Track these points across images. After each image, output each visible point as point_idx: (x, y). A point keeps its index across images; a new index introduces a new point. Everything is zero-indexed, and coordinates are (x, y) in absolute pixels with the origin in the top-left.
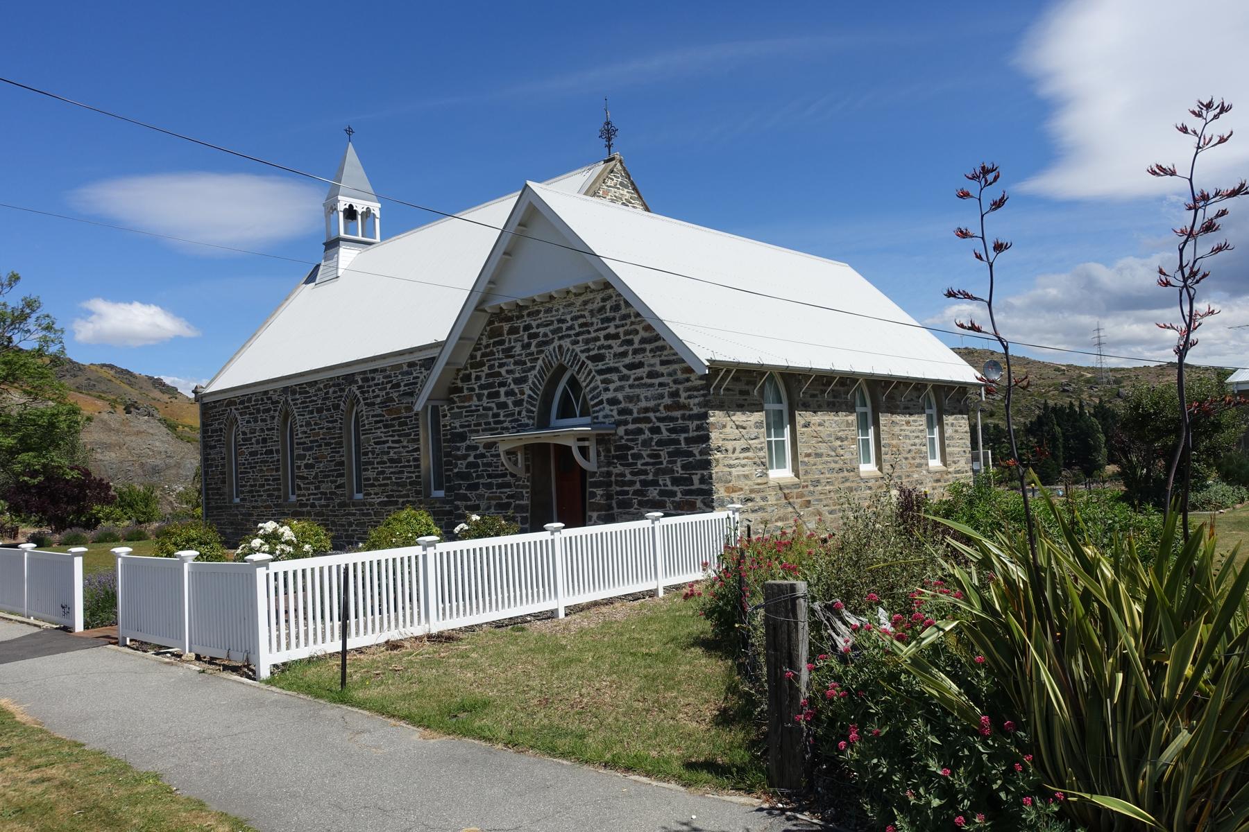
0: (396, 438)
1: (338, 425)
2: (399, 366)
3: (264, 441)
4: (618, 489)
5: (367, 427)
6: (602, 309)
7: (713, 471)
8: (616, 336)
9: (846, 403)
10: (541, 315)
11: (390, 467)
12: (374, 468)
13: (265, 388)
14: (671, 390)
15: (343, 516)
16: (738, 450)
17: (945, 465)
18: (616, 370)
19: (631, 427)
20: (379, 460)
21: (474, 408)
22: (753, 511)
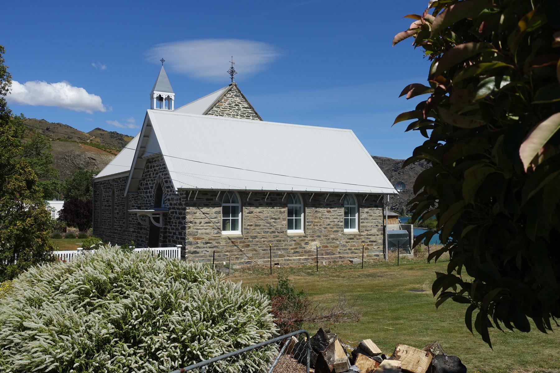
22: (210, 248)
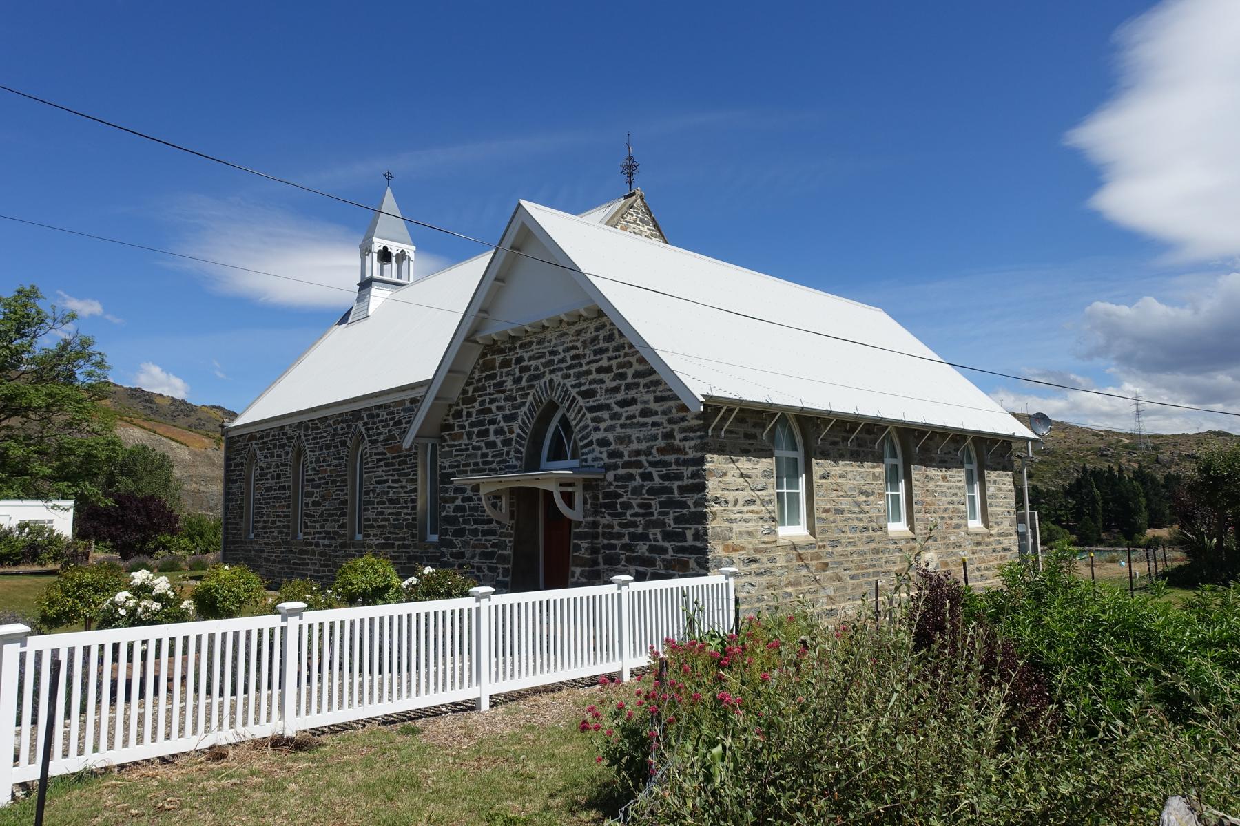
0: (396, 477)
1: (343, 462)
2: (402, 402)
3: (278, 476)
4: (606, 542)
5: (369, 466)
6: (594, 340)
7: (709, 526)
8: (608, 370)
9: (873, 453)
10: (533, 347)
11: (388, 508)
12: (373, 508)
13: (282, 423)
14: (664, 430)
15: (343, 557)
16: (741, 502)
17: (987, 526)
18: (607, 407)
19: (621, 471)
20: (379, 500)
21: (463, 447)
22: (757, 574)
